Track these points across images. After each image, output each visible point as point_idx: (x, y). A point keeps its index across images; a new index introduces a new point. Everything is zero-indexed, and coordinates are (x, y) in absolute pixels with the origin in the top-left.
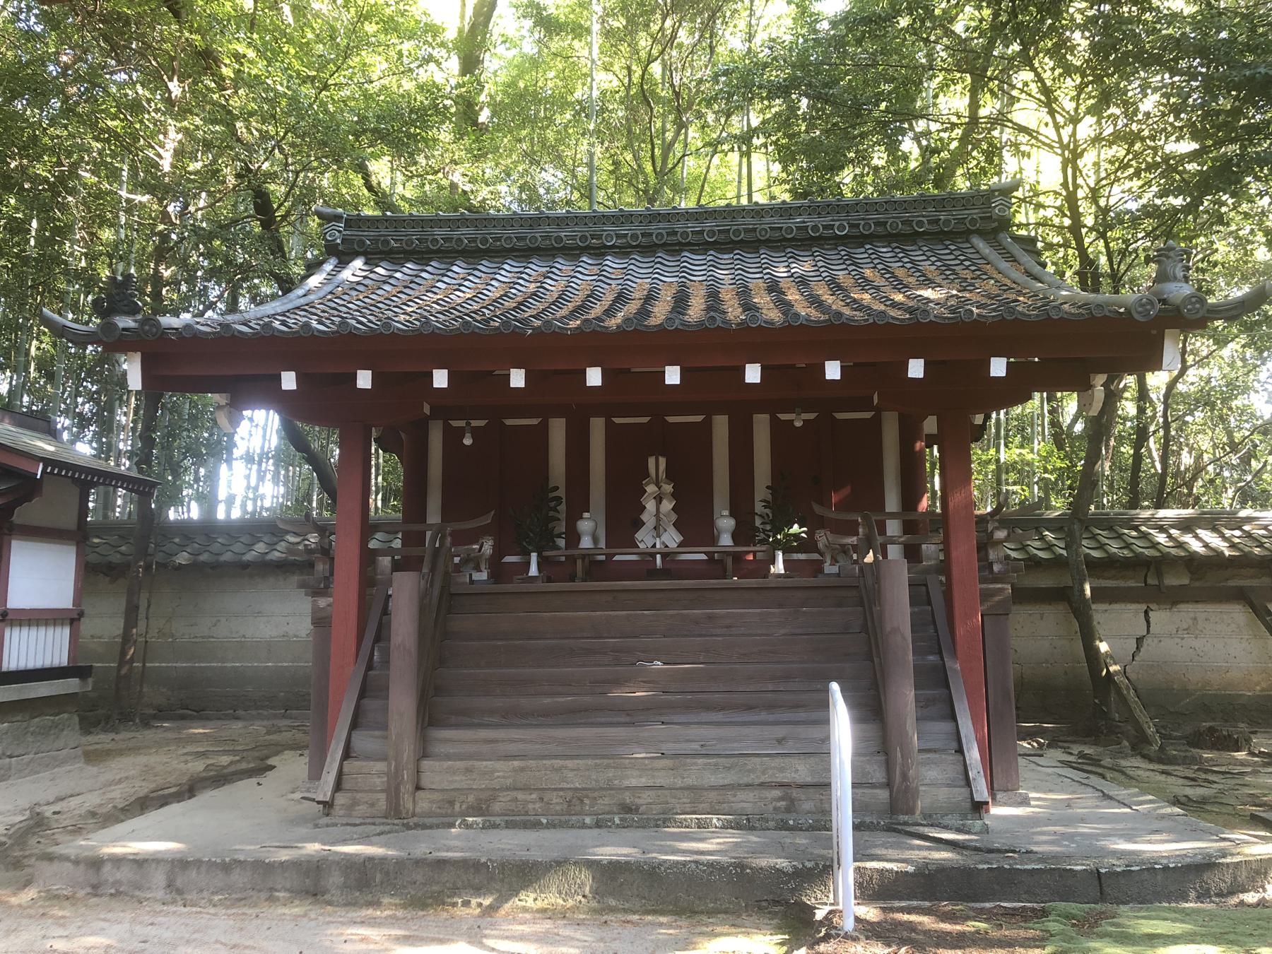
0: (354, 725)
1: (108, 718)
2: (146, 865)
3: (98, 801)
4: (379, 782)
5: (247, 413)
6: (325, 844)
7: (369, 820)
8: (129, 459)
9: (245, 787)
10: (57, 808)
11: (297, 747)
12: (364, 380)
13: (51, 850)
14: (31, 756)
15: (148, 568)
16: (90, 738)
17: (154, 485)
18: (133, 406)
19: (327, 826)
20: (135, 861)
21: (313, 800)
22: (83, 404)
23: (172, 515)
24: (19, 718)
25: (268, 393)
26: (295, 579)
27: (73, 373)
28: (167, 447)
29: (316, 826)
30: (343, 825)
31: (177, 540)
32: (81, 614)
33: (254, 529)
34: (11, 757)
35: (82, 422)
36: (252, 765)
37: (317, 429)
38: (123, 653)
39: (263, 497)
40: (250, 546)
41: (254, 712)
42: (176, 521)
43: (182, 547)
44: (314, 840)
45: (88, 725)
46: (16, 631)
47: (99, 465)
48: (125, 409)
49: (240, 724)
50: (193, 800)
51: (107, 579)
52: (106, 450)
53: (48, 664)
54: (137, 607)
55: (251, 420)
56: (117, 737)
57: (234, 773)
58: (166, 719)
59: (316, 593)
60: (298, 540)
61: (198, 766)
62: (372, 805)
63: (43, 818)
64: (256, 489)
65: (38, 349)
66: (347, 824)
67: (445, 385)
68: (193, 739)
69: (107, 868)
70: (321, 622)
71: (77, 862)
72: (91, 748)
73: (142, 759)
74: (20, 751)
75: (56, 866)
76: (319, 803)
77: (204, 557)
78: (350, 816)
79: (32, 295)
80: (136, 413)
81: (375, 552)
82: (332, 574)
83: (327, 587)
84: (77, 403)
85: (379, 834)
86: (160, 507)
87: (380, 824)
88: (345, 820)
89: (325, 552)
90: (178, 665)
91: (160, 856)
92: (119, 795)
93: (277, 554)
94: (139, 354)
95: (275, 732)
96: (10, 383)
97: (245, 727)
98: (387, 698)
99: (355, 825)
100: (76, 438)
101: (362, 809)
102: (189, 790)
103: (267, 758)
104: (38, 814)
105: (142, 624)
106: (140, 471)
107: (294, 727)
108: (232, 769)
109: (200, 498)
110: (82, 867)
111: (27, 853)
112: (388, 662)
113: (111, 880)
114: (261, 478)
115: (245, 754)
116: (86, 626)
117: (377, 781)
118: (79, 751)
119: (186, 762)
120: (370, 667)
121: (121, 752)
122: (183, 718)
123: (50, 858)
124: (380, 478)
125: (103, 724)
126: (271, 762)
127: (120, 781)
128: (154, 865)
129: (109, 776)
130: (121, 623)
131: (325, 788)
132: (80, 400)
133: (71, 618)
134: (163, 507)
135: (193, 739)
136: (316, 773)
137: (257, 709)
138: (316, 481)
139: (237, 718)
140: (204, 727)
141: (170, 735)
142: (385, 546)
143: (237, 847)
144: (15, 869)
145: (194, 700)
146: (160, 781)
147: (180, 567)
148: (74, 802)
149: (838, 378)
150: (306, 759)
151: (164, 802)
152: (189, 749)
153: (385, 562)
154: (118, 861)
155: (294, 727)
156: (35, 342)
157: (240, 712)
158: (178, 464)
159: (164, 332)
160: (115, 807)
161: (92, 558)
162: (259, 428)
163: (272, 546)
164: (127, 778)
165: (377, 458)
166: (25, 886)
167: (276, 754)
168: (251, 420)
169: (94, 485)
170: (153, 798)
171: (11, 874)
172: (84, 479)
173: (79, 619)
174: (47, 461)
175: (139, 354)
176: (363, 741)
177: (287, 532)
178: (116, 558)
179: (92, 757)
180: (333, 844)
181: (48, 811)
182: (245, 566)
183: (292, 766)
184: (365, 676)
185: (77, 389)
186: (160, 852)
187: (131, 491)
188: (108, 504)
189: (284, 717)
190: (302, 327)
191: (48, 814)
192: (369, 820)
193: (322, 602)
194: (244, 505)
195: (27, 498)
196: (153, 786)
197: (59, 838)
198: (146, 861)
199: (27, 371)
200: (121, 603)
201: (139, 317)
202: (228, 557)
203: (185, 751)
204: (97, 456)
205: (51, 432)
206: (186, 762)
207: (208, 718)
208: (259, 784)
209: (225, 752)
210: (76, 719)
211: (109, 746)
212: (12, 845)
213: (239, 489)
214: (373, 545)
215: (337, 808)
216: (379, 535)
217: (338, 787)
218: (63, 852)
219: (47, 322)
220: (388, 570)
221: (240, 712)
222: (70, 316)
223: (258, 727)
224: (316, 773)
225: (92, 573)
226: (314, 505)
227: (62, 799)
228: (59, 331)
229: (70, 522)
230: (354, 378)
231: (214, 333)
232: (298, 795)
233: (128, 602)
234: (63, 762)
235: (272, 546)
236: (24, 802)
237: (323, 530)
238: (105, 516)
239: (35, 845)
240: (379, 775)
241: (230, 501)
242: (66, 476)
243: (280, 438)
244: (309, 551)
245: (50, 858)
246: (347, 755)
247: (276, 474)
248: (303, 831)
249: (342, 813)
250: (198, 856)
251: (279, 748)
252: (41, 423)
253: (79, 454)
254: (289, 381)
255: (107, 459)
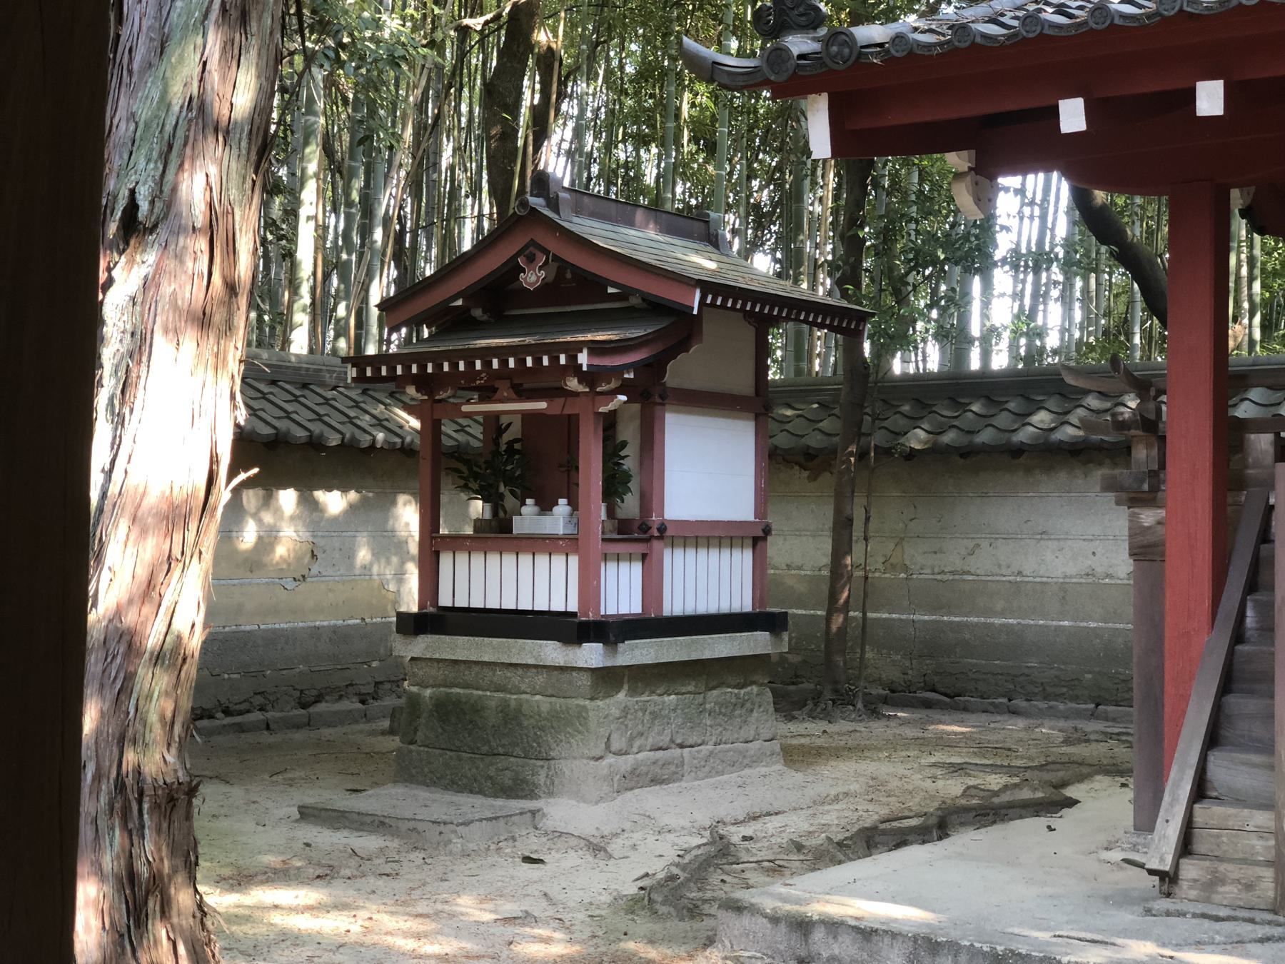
0: (1213, 740)
1: (817, 697)
2: (875, 938)
3: (806, 827)
4: (1262, 847)
5: (1002, 181)
6: (1164, 945)
7: (1246, 914)
8: (830, 274)
9: (1032, 826)
10: (748, 830)
11: (1115, 770)
12: (1210, 99)
13: (741, 894)
14: (710, 747)
15: (862, 455)
16: (794, 727)
17: (863, 317)
18: (832, 185)
19: (1168, 914)
20: (856, 929)
21: (1142, 866)
22: (761, 189)
23: (897, 367)
24: (691, 688)
25: (1028, 141)
26: (1099, 474)
27: (744, 142)
28: (884, 251)
29: (1148, 912)
30: (1195, 916)
31: (906, 408)
32: (767, 531)
33: (1033, 384)
34: (682, 746)
35: (760, 219)
36: (1040, 795)
37: (1139, 200)
38: (833, 595)
39: (1041, 333)
40: (1023, 417)
41: (1042, 705)
42: (905, 377)
43: (915, 421)
44: (1143, 935)
45: (790, 703)
46: (679, 552)
47: (784, 288)
48: (820, 193)
49: (1021, 723)
50: (945, 842)
51: (806, 474)
52: (791, 263)
53: (725, 608)
54: (850, 520)
55: (1021, 192)
56: (831, 728)
57: (1011, 805)
58: (903, 705)
59: (1137, 500)
60: (1108, 405)
61: (953, 788)
62: (1249, 887)
63: (729, 843)
64: (1032, 316)
65: (693, 105)
66: (1204, 916)
67: (1219, 111)
68: (944, 742)
69: (818, 935)
70: (1146, 551)
71: (775, 920)
72: (795, 742)
73: (868, 767)
74: (694, 739)
75: (746, 921)
76: (1152, 872)
77: (949, 438)
78: (1207, 901)
79: (678, 18)
80: (836, 198)
81: (1244, 426)
82: (1162, 465)
83: (1155, 489)
84: (750, 188)
85: (1262, 940)
86: (877, 353)
87: (1264, 923)
88: (1200, 908)
89: (1150, 425)
90: (916, 617)
91: (894, 927)
92: (836, 821)
93: (1070, 431)
94: (825, 96)
95: (1079, 741)
96: (658, 166)
97: (1027, 729)
98: (1272, 697)
99: (1218, 919)
100: (752, 247)
101: (1229, 892)
102: (938, 826)
103: (1064, 784)
104: (721, 837)
105: (858, 548)
106: (844, 294)
107: (1110, 736)
108: (1006, 797)
109: (942, 335)
110: (783, 927)
111: (709, 895)
112: (1272, 630)
113: (825, 955)
114: (1040, 296)
115: (1028, 775)
116: (777, 549)
117: (1258, 845)
118: (776, 745)
119: (934, 779)
120: (1238, 636)
121: (836, 753)
122: (928, 705)
123: (738, 908)
124: (1257, 286)
125: (810, 705)
126: (1071, 792)
127: (836, 799)
128: (887, 940)
129: (821, 789)
130: (827, 545)
131: (1162, 850)
132: (755, 184)
133: (755, 537)
134: (883, 352)
135: (944, 742)
136: (1146, 821)
137: (1046, 697)
138: (1138, 296)
139: (1015, 712)
140: (960, 723)
141: (910, 732)
142: (1003, 438)
143: (1016, 930)
144: (692, 917)
145: (943, 678)
146: (894, 805)
147: (911, 455)
148: (772, 824)
149: (1221, 82)
150: (1129, 794)
151: (900, 840)
152: (938, 757)
153: (1262, 443)
154: (834, 926)
155: (1110, 736)
156: (687, 96)
157: (1020, 703)
158: (903, 280)
159: (862, 52)
160: (829, 839)
161: (782, 441)
162: (1030, 208)
163: (1062, 418)
164: (846, 794)
165: (1251, 247)
166: (706, 946)
167: (1081, 778)
168: (1021, 192)
169: (775, 321)
170: (884, 832)
171: (686, 925)
172: (761, 311)
173: (765, 539)
174: (707, 287)
175: (825, 96)
176: (1223, 769)
177: (1087, 392)
178: (815, 441)
179: (796, 756)
180: (1178, 946)
181: (735, 834)
182: (1017, 452)
183: (1105, 804)
184: (1231, 654)
185: (749, 166)
186: (896, 921)
187: (831, 328)
188: (800, 353)
189: (1093, 716)
190: (1093, 12)
191: (736, 839)
192: (1246, 914)
193: (1148, 517)
194: (1013, 346)
195: (682, 345)
196: (884, 812)
197: (753, 877)
198: (874, 931)
199: (679, 146)
200: (828, 512)
201: (823, 31)
202: (986, 436)
203: (932, 760)
204: (779, 275)
205: (712, 240)
206: (934, 779)
207: (966, 709)
208: (1050, 829)
209: (994, 768)
210: (769, 695)
211: (819, 742)
212: (688, 880)
213: (1002, 313)
214: (1244, 411)
215: (1184, 885)
216: (1255, 394)
217: (1186, 847)
218: (753, 901)
219: (694, 62)
220: (1269, 458)
221: (1020, 703)
222: (734, 44)
223: (1048, 730)
224: (1146, 821)
225: (781, 463)
226: (1137, 340)
227: (755, 818)
228: (710, 72)
229: (742, 383)
230: (1054, 113)
231: (941, 44)
232: (1116, 855)
233: (838, 511)
234: (755, 761)
235: (1062, 418)
236: (704, 817)
237: (1144, 385)
238: (798, 372)
239: (719, 884)
240: (1261, 833)
241: (990, 335)
242: (733, 308)
243: (1073, 223)
244: (1121, 426)
245: (738, 908)
246: (1200, 791)
247: (1068, 285)
248: (1128, 917)
249: (1193, 894)
250: (955, 935)
251: (1085, 771)
252: (696, 225)
253: (752, 272)
254: (1072, 116)
255: (796, 281)
